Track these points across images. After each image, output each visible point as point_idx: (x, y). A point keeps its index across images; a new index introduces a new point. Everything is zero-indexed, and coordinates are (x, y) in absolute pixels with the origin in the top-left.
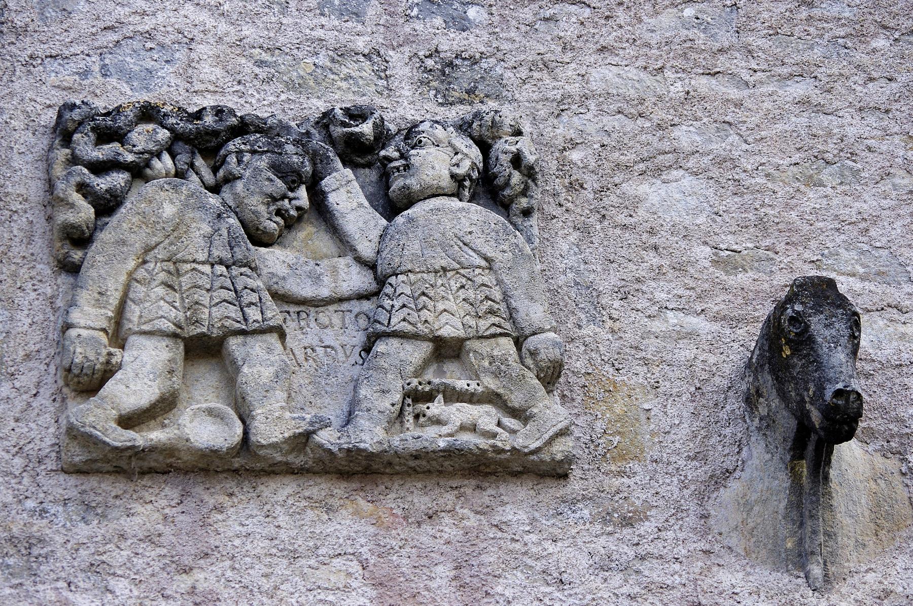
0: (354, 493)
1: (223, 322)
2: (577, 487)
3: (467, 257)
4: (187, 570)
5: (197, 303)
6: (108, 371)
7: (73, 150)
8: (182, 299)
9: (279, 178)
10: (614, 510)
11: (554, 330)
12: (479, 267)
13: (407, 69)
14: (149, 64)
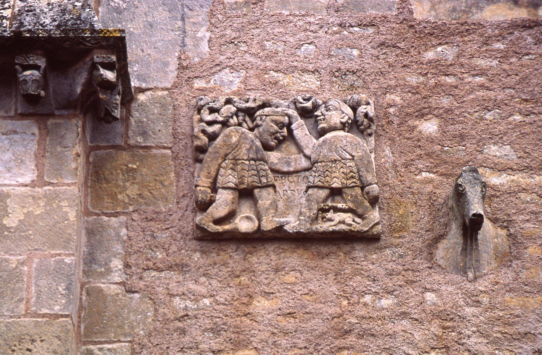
2: (382, 243)
4: (238, 277)
6: (211, 202)
8: (238, 174)
10: (396, 252)
11: (376, 183)
14: (231, 79)
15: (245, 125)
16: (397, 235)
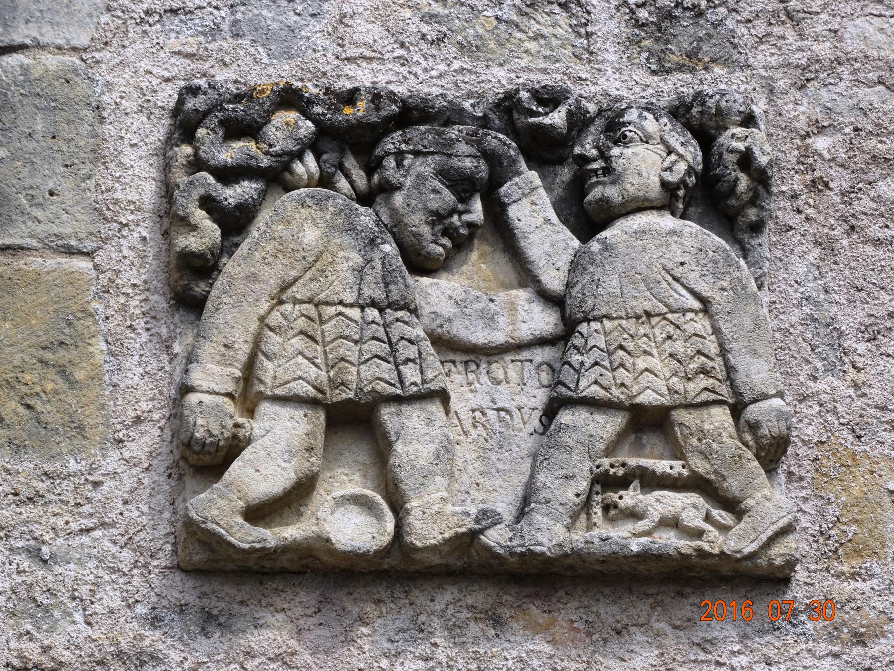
0: (527, 600)
1: (373, 384)
2: (799, 595)
3: (677, 296)
5: (343, 359)
7: (196, 150)
8: (325, 353)
9: (447, 187)
12: (692, 310)
13: (613, 24)
15: (343, 184)
16: (845, 568)
